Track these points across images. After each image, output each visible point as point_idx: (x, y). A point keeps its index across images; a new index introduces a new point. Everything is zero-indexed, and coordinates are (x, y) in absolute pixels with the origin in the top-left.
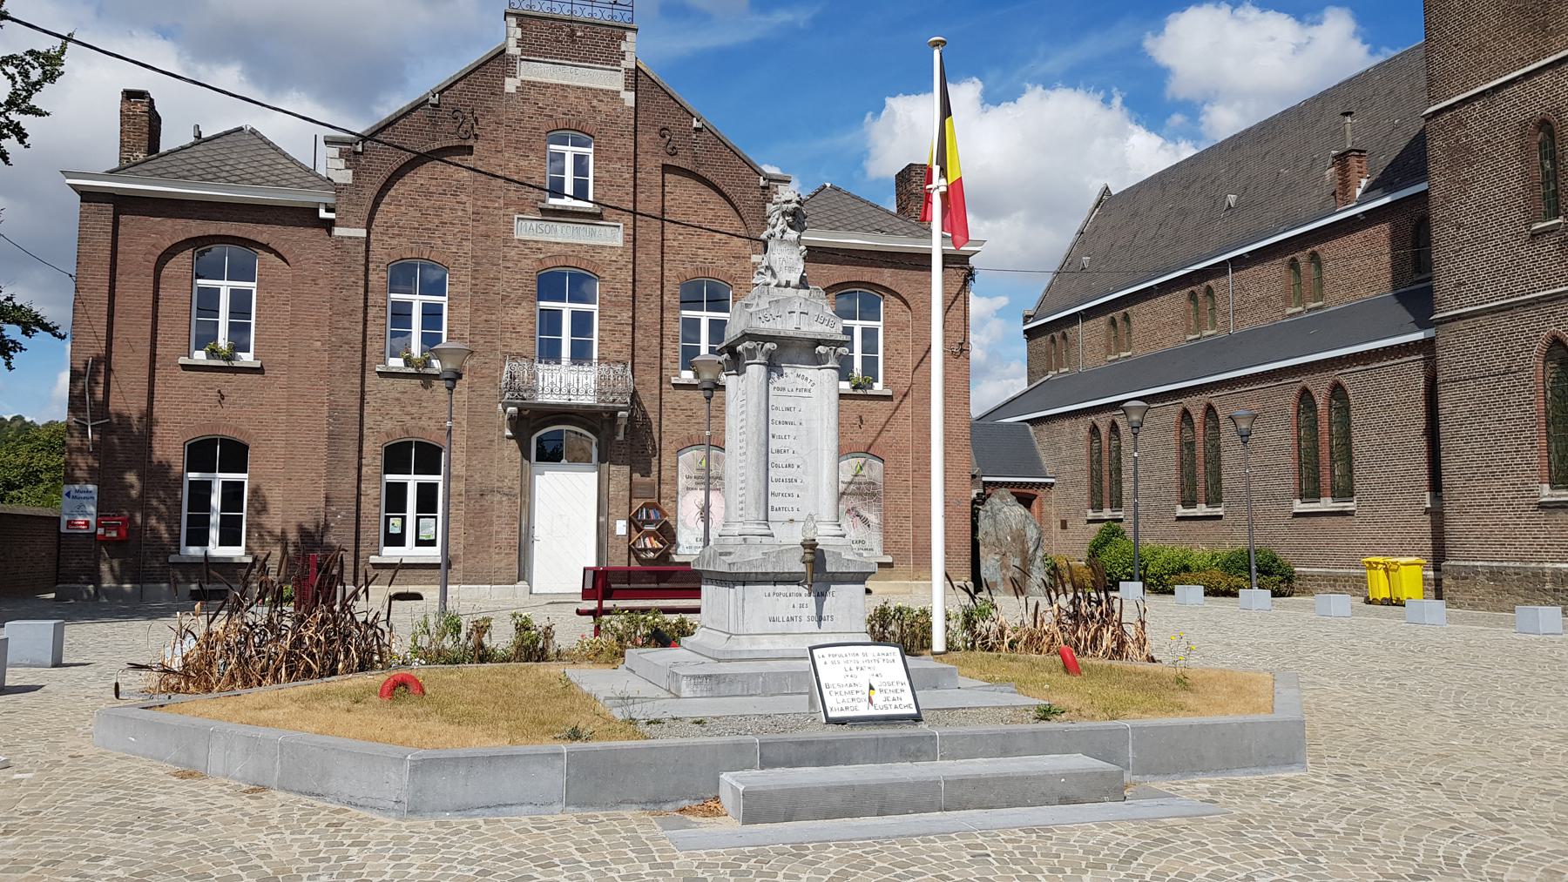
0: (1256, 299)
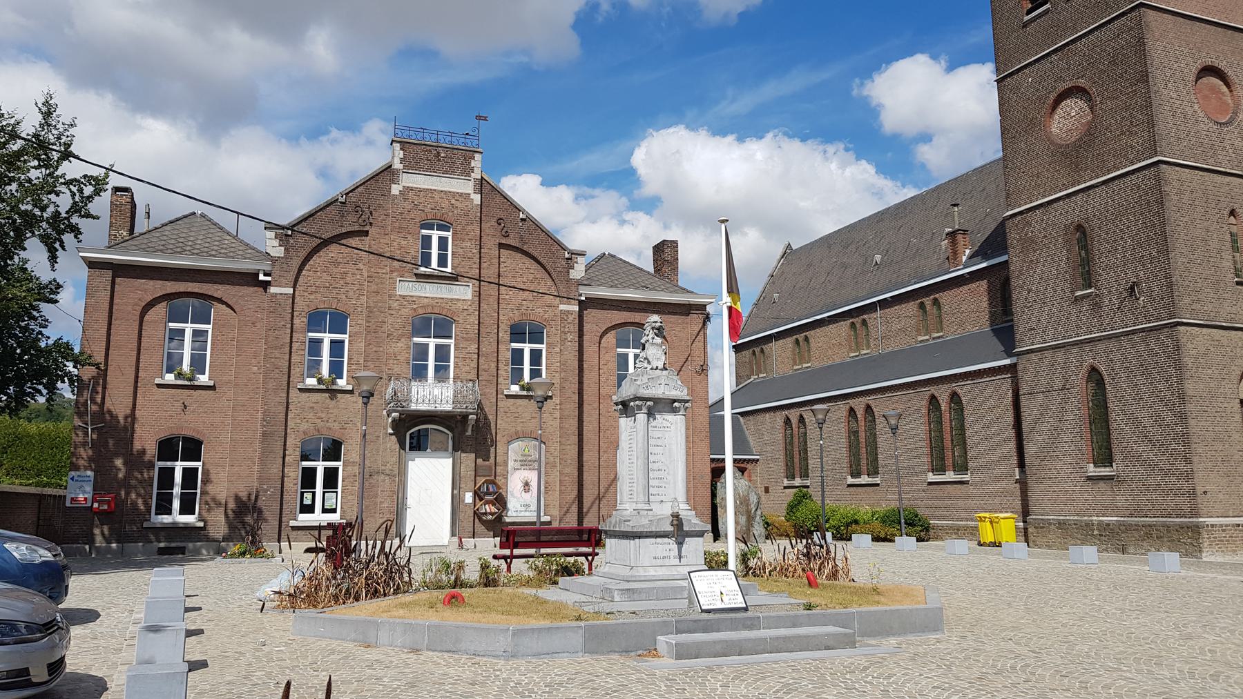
0: (896, 331)
